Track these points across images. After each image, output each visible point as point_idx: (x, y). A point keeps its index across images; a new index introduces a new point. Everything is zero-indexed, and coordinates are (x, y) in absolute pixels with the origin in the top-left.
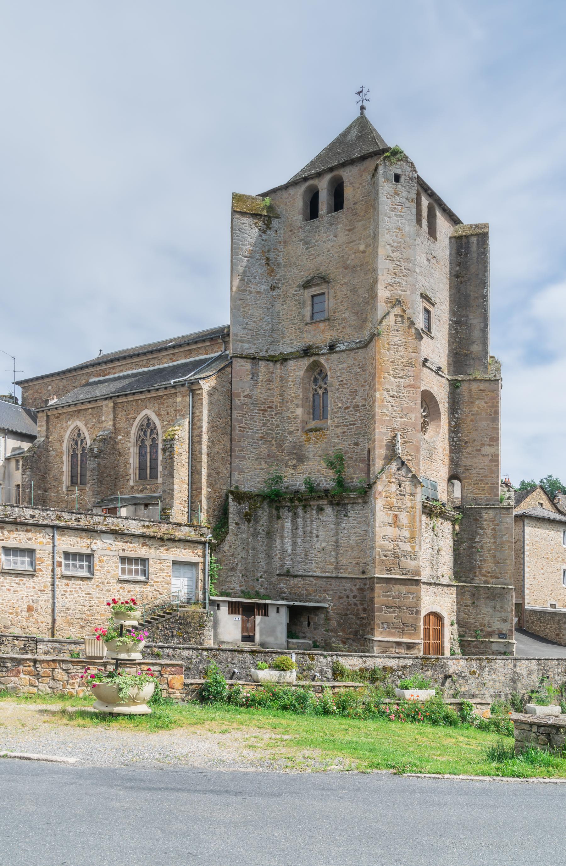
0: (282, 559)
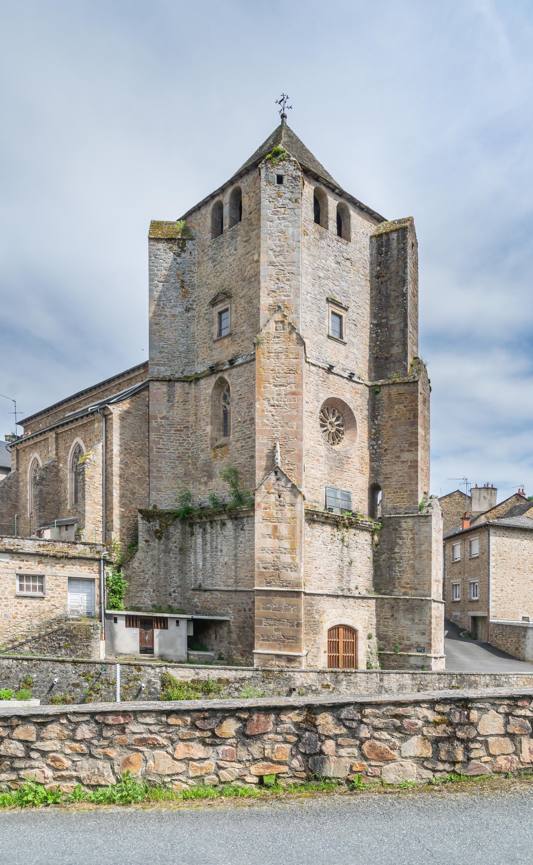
0: (195, 574)
